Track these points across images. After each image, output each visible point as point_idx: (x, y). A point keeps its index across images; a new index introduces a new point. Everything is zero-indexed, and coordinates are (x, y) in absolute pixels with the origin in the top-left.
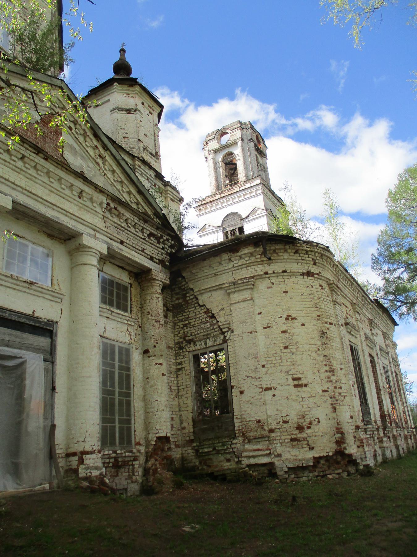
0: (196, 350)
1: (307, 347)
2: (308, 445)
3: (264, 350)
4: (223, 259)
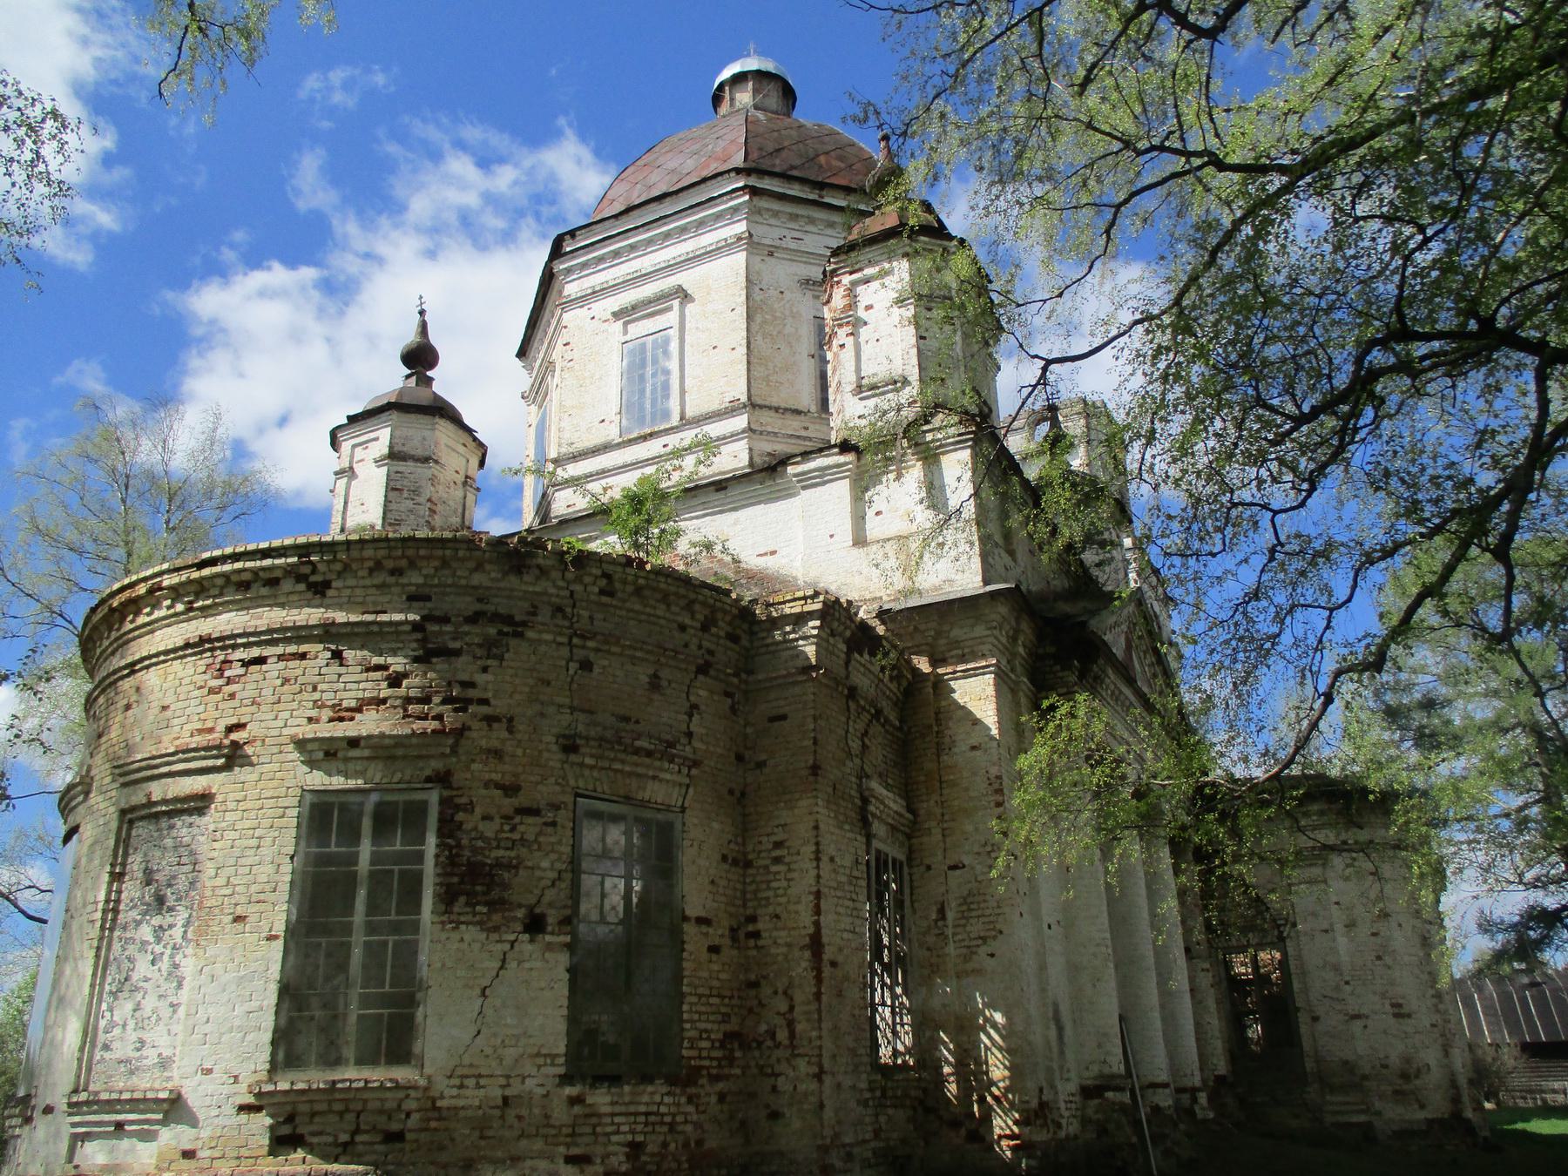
1: (1406, 958)
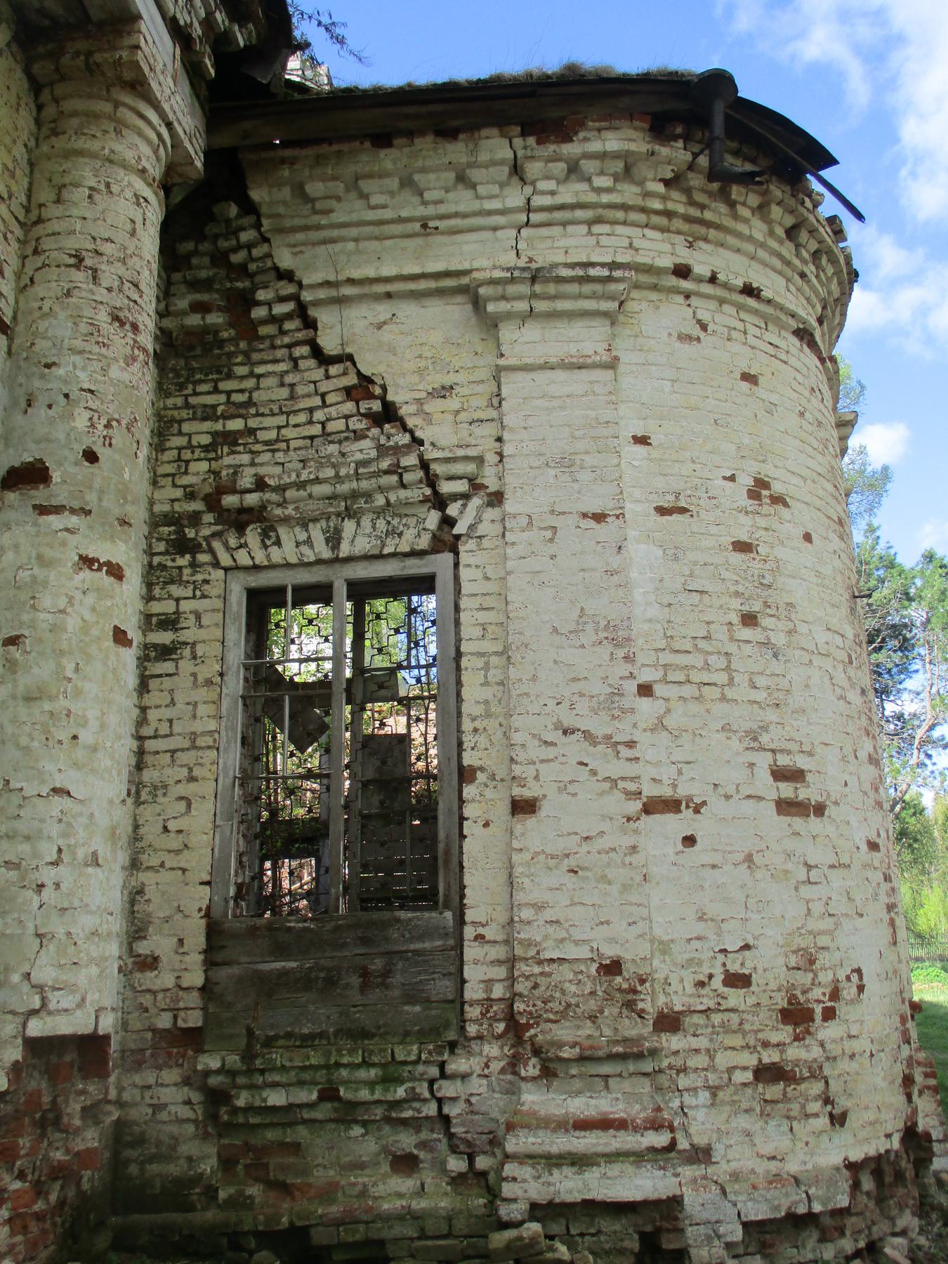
0: (273, 567)
2: (827, 1101)
3: (654, 611)
4: (484, 157)
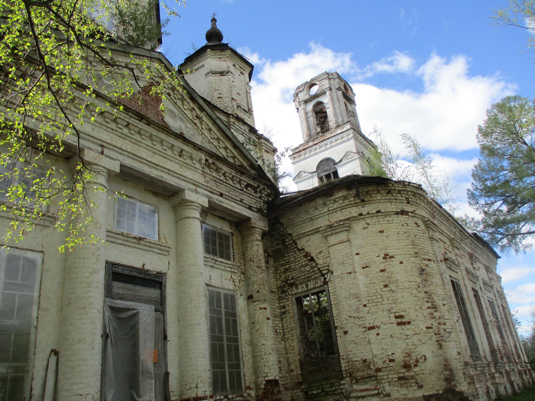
0: (298, 293)
1: (407, 285)
3: (365, 289)
4: (318, 204)
